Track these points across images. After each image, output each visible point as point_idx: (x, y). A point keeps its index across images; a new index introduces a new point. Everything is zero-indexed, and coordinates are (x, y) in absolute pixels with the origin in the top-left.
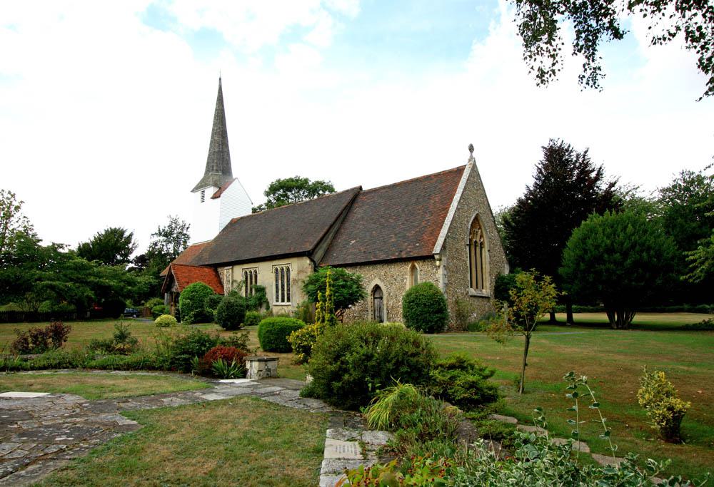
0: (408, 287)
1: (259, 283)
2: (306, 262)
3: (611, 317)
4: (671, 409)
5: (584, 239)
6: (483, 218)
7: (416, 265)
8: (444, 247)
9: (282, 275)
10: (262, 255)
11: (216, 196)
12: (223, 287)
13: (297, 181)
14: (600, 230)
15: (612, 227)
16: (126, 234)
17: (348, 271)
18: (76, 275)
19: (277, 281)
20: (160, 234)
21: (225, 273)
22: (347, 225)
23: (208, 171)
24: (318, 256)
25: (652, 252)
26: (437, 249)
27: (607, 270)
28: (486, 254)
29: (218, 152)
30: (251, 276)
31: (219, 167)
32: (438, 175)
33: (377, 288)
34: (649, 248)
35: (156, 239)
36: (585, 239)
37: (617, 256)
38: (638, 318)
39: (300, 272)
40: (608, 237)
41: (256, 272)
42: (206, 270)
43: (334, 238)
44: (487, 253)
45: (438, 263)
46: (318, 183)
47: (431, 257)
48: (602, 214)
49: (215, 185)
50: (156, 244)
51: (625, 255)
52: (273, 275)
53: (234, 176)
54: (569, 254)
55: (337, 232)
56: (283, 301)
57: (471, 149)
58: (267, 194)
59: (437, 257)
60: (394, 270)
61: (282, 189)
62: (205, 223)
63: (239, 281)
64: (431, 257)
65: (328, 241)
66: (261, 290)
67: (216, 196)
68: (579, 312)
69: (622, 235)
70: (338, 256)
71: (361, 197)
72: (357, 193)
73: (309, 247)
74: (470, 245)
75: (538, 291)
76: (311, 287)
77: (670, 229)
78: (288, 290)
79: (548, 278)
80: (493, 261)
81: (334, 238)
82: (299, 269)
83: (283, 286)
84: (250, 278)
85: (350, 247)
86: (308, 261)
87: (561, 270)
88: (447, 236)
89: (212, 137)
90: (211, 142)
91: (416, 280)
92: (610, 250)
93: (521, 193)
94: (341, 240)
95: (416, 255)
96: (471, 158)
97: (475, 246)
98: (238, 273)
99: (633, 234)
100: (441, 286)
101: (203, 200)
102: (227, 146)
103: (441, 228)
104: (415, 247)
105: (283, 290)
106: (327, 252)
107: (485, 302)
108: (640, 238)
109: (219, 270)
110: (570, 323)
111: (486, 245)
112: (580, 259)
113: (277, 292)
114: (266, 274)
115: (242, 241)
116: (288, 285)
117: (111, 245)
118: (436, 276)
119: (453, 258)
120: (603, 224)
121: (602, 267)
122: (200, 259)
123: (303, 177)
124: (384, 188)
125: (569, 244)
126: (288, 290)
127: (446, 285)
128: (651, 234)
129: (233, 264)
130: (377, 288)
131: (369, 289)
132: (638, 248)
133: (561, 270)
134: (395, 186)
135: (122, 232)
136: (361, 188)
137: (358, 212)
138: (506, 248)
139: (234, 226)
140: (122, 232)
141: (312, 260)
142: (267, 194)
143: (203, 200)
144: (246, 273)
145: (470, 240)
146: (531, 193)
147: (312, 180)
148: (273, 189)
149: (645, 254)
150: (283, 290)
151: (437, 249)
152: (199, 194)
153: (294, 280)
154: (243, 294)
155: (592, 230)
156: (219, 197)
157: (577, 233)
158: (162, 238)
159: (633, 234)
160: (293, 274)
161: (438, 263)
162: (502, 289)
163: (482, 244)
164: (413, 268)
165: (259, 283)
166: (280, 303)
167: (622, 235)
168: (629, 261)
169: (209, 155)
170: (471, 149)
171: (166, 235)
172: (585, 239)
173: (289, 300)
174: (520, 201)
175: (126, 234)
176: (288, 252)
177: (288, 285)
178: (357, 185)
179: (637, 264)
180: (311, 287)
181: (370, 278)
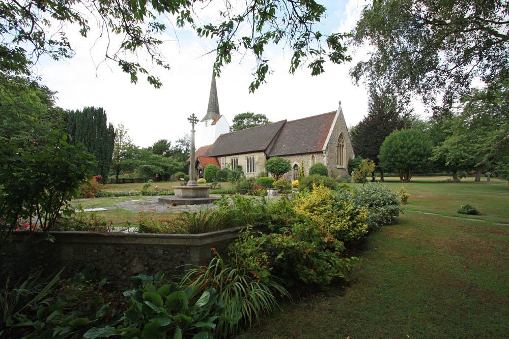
0: (310, 165)
1: (239, 164)
2: (263, 154)
3: (401, 178)
4: (404, 196)
5: (390, 142)
6: (344, 134)
7: (314, 155)
8: (327, 148)
9: (251, 163)
10: (240, 151)
11: (213, 124)
12: (220, 166)
13: (248, 114)
14: (398, 138)
15: (404, 136)
16: (168, 143)
17: (284, 158)
18: (154, 162)
19: (248, 163)
20: (180, 142)
21: (221, 160)
22: (280, 138)
23: (208, 111)
24: (268, 152)
25: (422, 148)
26: (324, 149)
27: (401, 156)
28: (344, 150)
29: (213, 102)
30: (235, 162)
31: (214, 110)
32: (324, 115)
33: (296, 165)
34: (420, 146)
35: (178, 144)
36: (391, 142)
37: (405, 150)
38: (413, 179)
39: (259, 159)
40: (402, 141)
41: (237, 159)
42: (213, 159)
43: (275, 143)
44: (345, 150)
45: (324, 154)
46: (259, 115)
47: (321, 152)
48: (400, 130)
49: (213, 119)
50: (177, 146)
51: (409, 149)
52: (246, 161)
53: (221, 114)
54: (383, 149)
55: (276, 141)
56: (251, 172)
57: (340, 103)
58: (234, 121)
59: (324, 152)
60: (304, 158)
61: (240, 118)
62: (206, 137)
63: (229, 163)
64: (321, 152)
65: (272, 145)
66: (240, 167)
67: (213, 124)
68: (388, 177)
69: (408, 140)
70: (277, 152)
71: (287, 124)
72: (284, 123)
73: (264, 148)
74: (338, 146)
75: (367, 165)
76: (269, 166)
77: (432, 137)
78: (254, 167)
79: (372, 161)
80: (348, 153)
81: (275, 143)
82: (259, 158)
83: (251, 165)
84: (234, 162)
85: (283, 147)
86: (264, 154)
87: (378, 156)
88: (328, 143)
89: (210, 95)
90: (210, 98)
91: (314, 162)
92: (402, 147)
93: (362, 119)
94: (278, 144)
95: (314, 151)
96: (340, 107)
97: (340, 146)
98: (228, 160)
99: (413, 140)
100: (325, 164)
101: (206, 125)
102: (217, 99)
103: (326, 139)
104: (314, 148)
105: (251, 167)
106: (272, 150)
107: (344, 171)
108: (416, 141)
109: (218, 158)
110: (382, 181)
111: (345, 145)
112: (388, 151)
113: (248, 167)
114: (242, 160)
115: (225, 146)
116: (254, 165)
117: (161, 147)
118: (324, 160)
119: (331, 152)
120: (400, 135)
121: (398, 155)
122: (208, 154)
123: (251, 112)
124: (298, 120)
125: (383, 144)
126: (254, 167)
127: (328, 164)
128: (422, 139)
129: (225, 156)
130: (296, 165)
131: (292, 166)
132: (415, 146)
133: (378, 156)
134: (303, 119)
135: (166, 141)
136: (286, 120)
137: (286, 131)
138: (353, 146)
139: (222, 138)
140: (166, 141)
141: (265, 154)
142: (234, 121)
143: (206, 125)
144: (232, 160)
145: (338, 144)
146: (367, 119)
147: (256, 113)
148: (236, 119)
149: (418, 149)
150: (251, 167)
151: (324, 149)
152: (204, 123)
153: (257, 163)
154: (231, 169)
155: (395, 138)
156: (215, 124)
157: (387, 139)
158: (180, 143)
159: (413, 140)
160: (256, 160)
161: (324, 154)
162: (351, 166)
163: (343, 145)
164: (313, 157)
165: (239, 164)
166: (252, 173)
167: (408, 140)
168: (411, 152)
169: (209, 104)
170: (340, 103)
171: (182, 142)
172: (391, 142)
173: (254, 171)
174: (360, 123)
175: (168, 143)
176: (253, 150)
177: (254, 165)
178: (284, 119)
179: (414, 154)
180: (269, 166)
181: (294, 161)
